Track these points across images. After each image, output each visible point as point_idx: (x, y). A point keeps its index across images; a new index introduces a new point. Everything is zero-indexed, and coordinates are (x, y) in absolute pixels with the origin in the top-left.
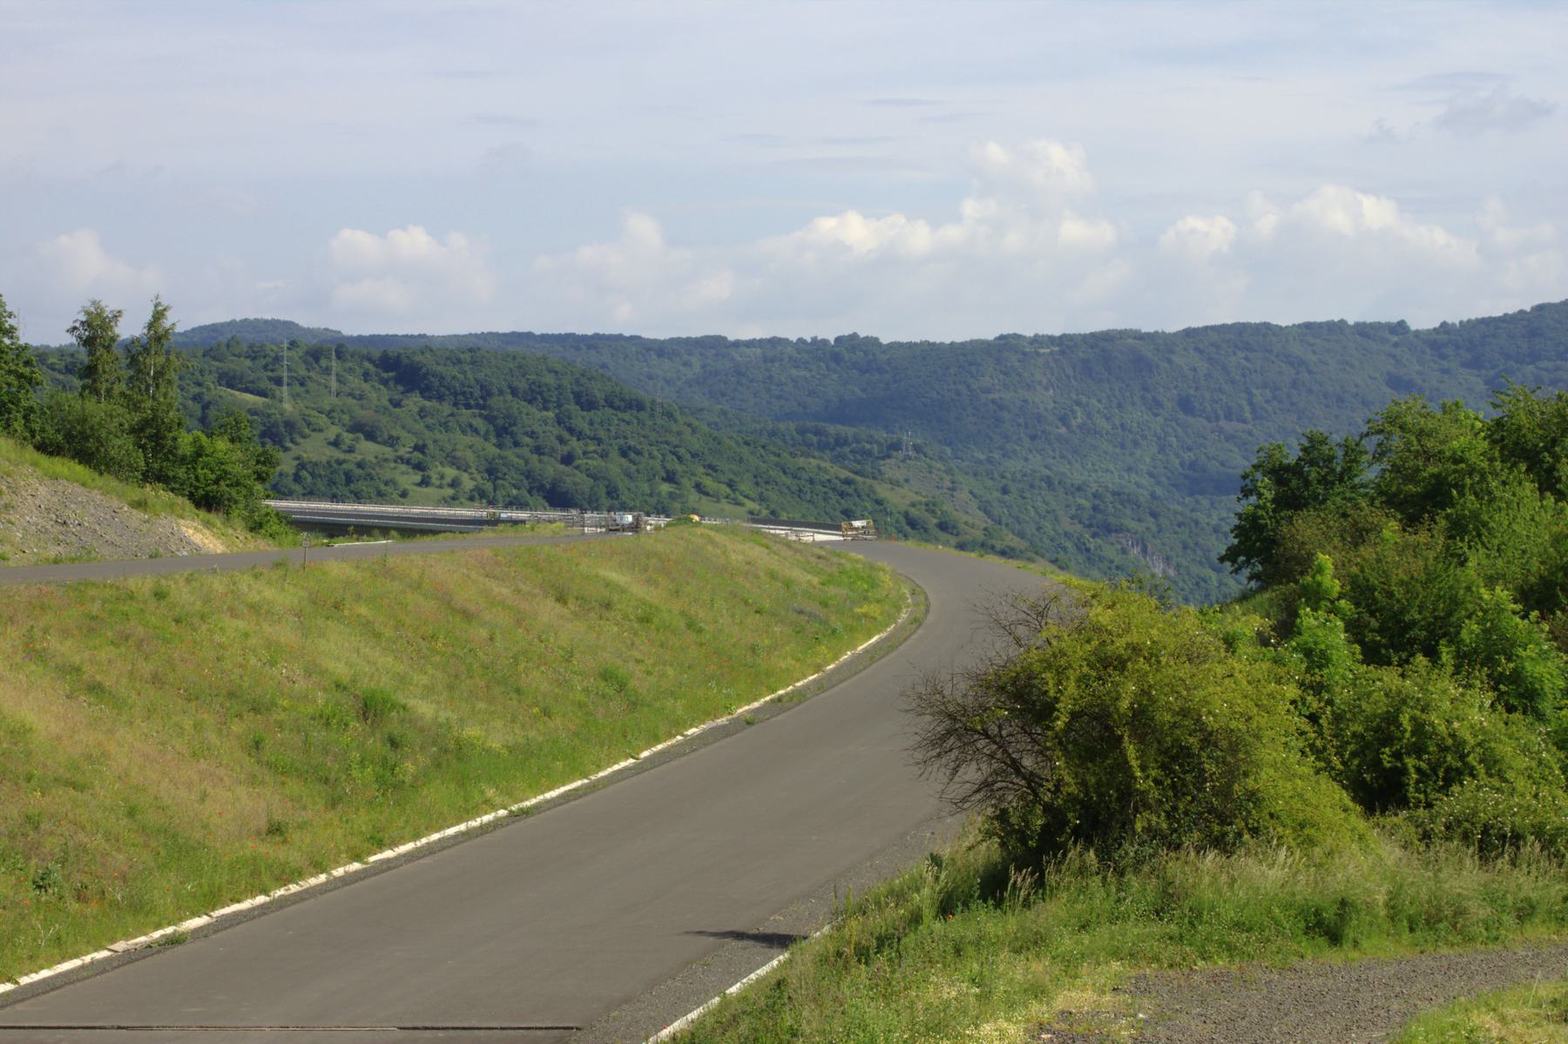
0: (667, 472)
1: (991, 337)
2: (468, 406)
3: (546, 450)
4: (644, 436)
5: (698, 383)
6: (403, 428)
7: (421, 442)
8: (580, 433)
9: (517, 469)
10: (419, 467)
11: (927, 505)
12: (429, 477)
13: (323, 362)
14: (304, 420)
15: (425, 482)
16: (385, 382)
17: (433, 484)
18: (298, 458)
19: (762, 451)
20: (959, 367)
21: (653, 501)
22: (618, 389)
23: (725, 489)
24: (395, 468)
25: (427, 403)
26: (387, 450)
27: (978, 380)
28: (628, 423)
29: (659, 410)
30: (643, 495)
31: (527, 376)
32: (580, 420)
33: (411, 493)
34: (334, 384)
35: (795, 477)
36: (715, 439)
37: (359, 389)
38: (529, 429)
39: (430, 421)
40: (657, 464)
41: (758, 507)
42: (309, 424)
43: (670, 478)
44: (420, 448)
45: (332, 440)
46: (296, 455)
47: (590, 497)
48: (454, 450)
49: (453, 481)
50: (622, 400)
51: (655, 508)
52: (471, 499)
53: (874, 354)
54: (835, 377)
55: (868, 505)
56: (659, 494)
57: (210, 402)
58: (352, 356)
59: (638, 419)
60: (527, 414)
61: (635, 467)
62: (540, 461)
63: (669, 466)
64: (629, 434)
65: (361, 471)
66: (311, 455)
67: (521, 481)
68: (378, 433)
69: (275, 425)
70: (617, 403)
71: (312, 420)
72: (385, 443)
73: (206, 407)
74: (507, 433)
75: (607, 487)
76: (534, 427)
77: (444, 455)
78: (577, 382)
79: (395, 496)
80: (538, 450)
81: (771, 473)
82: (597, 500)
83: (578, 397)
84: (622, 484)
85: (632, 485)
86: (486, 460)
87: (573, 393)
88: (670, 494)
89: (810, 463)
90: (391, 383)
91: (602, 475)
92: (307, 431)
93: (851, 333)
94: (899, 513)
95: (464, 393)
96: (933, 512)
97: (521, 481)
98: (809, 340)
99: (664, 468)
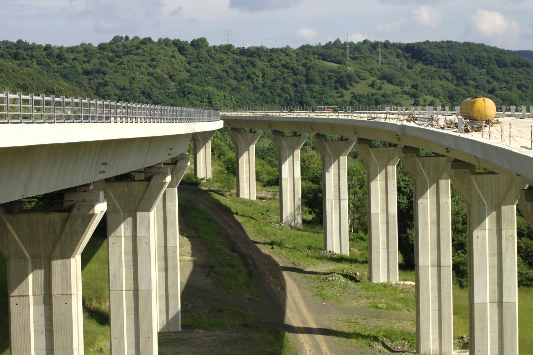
1: (462, 42)
2: (445, 68)
3: (481, 87)
4: (529, 80)
6: (408, 77)
7: (415, 84)
10: (414, 96)
12: (418, 101)
13: (377, 50)
14: (357, 74)
16: (406, 58)
18: (352, 93)
22: (517, 58)
24: (401, 97)
25: (425, 67)
26: (399, 88)
28: (522, 73)
32: (498, 72)
34: (380, 59)
38: (473, 77)
39: (423, 74)
42: (359, 76)
45: (370, 84)
46: (352, 92)
48: (432, 87)
49: (431, 102)
50: (520, 63)
57: (310, 67)
58: (392, 47)
60: (472, 70)
61: (524, 94)
65: (383, 99)
68: (394, 80)
69: (342, 77)
70: (517, 65)
72: (397, 85)
73: (308, 69)
74: (462, 79)
78: (498, 55)
83: (498, 62)
86: (448, 92)
87: (496, 60)
90: (410, 59)
91: (508, 98)
92: (358, 80)
95: (443, 62)
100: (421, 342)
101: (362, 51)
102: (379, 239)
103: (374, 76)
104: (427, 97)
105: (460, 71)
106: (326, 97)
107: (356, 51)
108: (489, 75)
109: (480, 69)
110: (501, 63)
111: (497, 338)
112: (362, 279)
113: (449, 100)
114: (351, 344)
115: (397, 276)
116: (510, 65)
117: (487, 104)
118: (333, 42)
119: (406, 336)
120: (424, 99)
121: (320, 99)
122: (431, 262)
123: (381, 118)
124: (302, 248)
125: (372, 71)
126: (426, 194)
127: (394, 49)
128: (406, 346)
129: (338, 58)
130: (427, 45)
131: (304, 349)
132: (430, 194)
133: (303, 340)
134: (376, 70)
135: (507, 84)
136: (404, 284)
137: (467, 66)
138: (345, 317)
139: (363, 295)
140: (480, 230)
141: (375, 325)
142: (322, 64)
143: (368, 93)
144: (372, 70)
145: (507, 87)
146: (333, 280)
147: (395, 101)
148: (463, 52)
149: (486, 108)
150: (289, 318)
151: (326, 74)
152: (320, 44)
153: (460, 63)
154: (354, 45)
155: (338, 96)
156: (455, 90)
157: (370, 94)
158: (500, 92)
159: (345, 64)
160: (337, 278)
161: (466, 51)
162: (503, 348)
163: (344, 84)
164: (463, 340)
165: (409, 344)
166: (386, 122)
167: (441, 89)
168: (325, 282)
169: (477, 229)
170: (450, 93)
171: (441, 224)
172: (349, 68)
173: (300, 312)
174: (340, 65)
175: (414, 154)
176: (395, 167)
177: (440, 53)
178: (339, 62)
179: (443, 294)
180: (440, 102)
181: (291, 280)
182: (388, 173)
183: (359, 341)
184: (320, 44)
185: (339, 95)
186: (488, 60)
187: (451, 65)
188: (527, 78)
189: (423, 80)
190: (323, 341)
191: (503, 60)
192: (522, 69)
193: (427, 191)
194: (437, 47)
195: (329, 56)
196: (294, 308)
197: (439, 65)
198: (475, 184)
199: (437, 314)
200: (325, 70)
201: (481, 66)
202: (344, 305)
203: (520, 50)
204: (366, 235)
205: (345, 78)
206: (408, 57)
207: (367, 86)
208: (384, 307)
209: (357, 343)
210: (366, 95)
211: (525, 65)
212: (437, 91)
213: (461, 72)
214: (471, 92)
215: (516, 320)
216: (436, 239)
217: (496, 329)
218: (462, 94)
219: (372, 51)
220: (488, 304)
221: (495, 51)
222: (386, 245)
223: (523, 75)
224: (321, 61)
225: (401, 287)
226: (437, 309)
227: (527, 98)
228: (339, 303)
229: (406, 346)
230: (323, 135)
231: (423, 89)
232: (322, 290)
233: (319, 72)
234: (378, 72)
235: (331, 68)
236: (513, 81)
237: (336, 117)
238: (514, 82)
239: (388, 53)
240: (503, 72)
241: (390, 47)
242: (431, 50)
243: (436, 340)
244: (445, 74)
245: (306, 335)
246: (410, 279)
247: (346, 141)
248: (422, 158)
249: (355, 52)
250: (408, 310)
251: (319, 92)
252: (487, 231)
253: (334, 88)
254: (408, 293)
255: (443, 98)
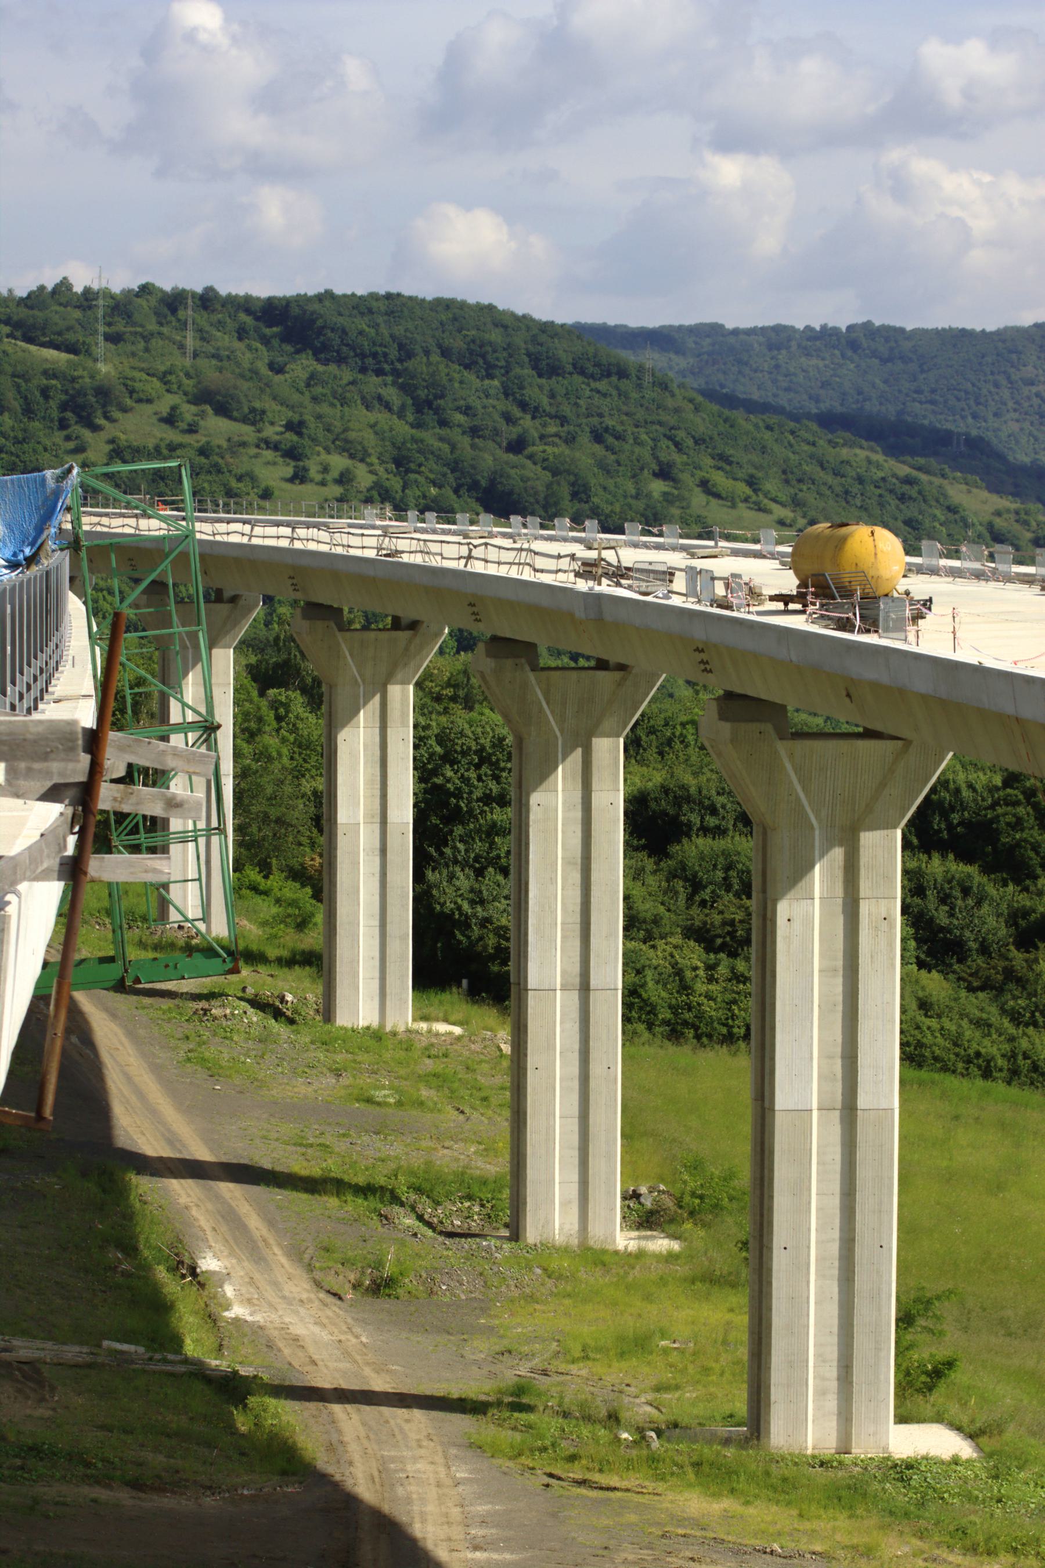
0: (660, 463)
2: (379, 372)
3: (487, 433)
4: (627, 414)
5: (693, 373)
6: (274, 399)
7: (296, 418)
8: (536, 409)
9: (439, 458)
10: (292, 454)
11: (1017, 513)
12: (306, 470)
13: (181, 314)
15: (299, 477)
16: (266, 341)
17: (312, 481)
18: (112, 441)
19: (791, 437)
20: (998, 355)
21: (640, 505)
22: (591, 350)
23: (742, 489)
24: (256, 456)
25: (320, 368)
27: (1019, 370)
28: (605, 395)
29: (648, 379)
30: (625, 497)
31: (464, 332)
32: (537, 391)
33: (276, 493)
34: (190, 341)
35: (836, 474)
36: (726, 421)
37: (228, 349)
38: (462, 403)
39: (319, 390)
40: (646, 453)
41: (791, 515)
42: (132, 392)
43: (664, 473)
44: (295, 427)
45: (165, 415)
47: (546, 498)
48: (346, 430)
49: (342, 475)
50: (597, 365)
51: (642, 515)
52: (368, 501)
53: (896, 342)
54: (852, 366)
55: (938, 513)
56: (649, 495)
58: (223, 306)
59: (617, 388)
60: (461, 382)
61: (613, 457)
62: (473, 446)
63: (663, 456)
64: (605, 410)
65: (203, 460)
66: (132, 437)
67: (444, 475)
68: (234, 405)
70: (591, 369)
71: (138, 385)
72: (244, 420)
74: (430, 407)
75: (573, 484)
76: (470, 400)
77: (331, 437)
78: (534, 340)
79: (253, 497)
80: (474, 432)
81: (805, 467)
82: (556, 504)
83: (535, 361)
84: (595, 480)
85: (610, 483)
86: (393, 444)
87: (529, 355)
88: (665, 494)
89: (856, 455)
90: (275, 342)
91: (566, 466)
92: (129, 402)
93: (865, 320)
94: (981, 524)
95: (374, 355)
96: (1026, 523)
97: (444, 475)
98: (818, 328)
99: (656, 458)
100: (528, 1209)
101: (137, 317)
102: (358, 899)
103: (176, 393)
104: (330, 457)
105: (425, 384)
106: (35, 451)
107: (119, 315)
108: (511, 398)
109: (482, 380)
110: (544, 363)
111: (838, 1211)
112: (300, 1014)
113: (395, 470)
114: (327, 1213)
115: (407, 1008)
116: (569, 368)
117: (880, 545)
118: (50, 287)
119: (475, 1189)
120: (321, 464)
121: (18, 456)
122: (562, 976)
123: (441, 555)
124: (91, 915)
125: (169, 377)
126: (552, 778)
127: (230, 313)
128: (476, 1217)
129: (71, 337)
130: (327, 303)
131: (197, 1224)
132: (564, 778)
133: (184, 1196)
134: (181, 374)
135: (562, 426)
136: (429, 1031)
137: (446, 371)
138: (288, 1129)
139: (318, 1061)
140: (797, 899)
141: (378, 1155)
142: (24, 351)
143: (158, 441)
144: (170, 373)
145: (562, 434)
146: (225, 1016)
147: (237, 467)
148: (434, 326)
149: (879, 556)
150: (125, 1130)
151: (35, 382)
152: (10, 291)
153: (425, 359)
154: (112, 297)
155: (69, 448)
156: (414, 440)
157: (163, 445)
158: (541, 448)
159: (88, 353)
160: (236, 1012)
161: (442, 324)
162: (853, 1240)
163: (89, 415)
164: (640, 1203)
165: (484, 1211)
166: (469, 569)
167: (372, 436)
168: (201, 1021)
169: (788, 897)
170: (399, 448)
171: (593, 866)
172: (103, 368)
173: (153, 1112)
174: (76, 358)
175: (523, 660)
176: (409, 690)
177: (367, 329)
178: (71, 349)
179: (596, 1069)
180: (369, 475)
181: (104, 1015)
182: (389, 707)
183: (346, 1202)
184: (10, 291)
185: (71, 445)
186: (505, 354)
187: (399, 366)
188: (619, 410)
189: (318, 409)
190: (245, 1203)
191: (551, 354)
192: (605, 381)
193: (556, 767)
194: (355, 312)
195: (44, 328)
196: (134, 1099)
197: (363, 363)
198: (788, 766)
199: (576, 1128)
200: (33, 370)
201: (486, 370)
202: (274, 1092)
203: (579, 323)
204: (266, 877)
205: (90, 397)
206: (272, 337)
207: (156, 422)
208: (392, 1100)
209: (342, 1207)
210: (151, 446)
211: (614, 370)
212: (360, 439)
213: (427, 387)
214: (459, 446)
215: (892, 1159)
216: (578, 909)
217: (836, 1187)
218: (432, 453)
219: (165, 317)
220: (815, 1114)
221: (528, 328)
222: (378, 917)
223: (608, 400)
224: (20, 343)
225: (425, 1041)
226: (577, 1114)
227: (621, 468)
228: (260, 1087)
229: (476, 1217)
230: (331, 607)
231: (321, 434)
232: (200, 1044)
233: (14, 375)
234: (185, 381)
235: (48, 366)
236: (578, 416)
237: (245, 540)
238: (584, 421)
239: (212, 325)
240: (551, 390)
241: (218, 307)
242: (340, 319)
243: (570, 1202)
244: (382, 391)
245: (189, 1183)
246: (441, 1015)
247: (411, 632)
248: (545, 673)
249: (116, 319)
250: (458, 1109)
251: (12, 434)
252: (817, 902)
253: (57, 423)
254: (445, 1060)
255: (377, 461)
